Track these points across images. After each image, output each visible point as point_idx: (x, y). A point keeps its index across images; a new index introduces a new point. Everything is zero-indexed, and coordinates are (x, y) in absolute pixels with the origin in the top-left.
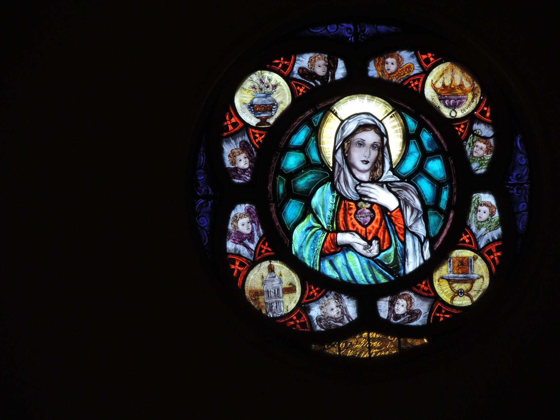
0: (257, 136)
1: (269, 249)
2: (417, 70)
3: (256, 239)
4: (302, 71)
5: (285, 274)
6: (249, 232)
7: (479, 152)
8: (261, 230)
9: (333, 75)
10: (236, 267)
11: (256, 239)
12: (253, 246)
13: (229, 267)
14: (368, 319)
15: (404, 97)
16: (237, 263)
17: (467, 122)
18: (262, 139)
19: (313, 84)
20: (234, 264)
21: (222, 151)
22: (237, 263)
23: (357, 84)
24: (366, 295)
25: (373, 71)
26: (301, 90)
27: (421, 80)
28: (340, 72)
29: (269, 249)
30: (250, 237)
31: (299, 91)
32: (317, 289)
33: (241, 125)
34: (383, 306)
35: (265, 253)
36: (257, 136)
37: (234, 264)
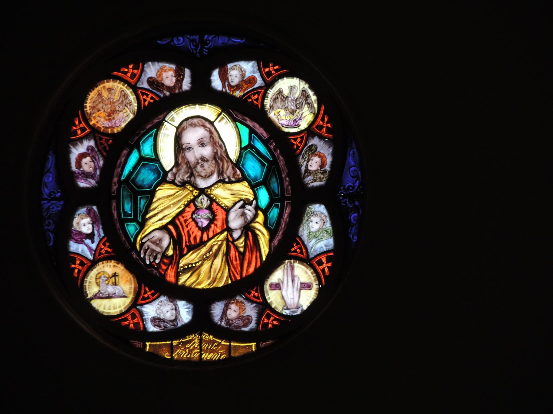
0: (298, 250)
1: (293, 141)
2: (260, 82)
3: (97, 239)
4: (151, 81)
5: (280, 116)
6: (90, 232)
7: (316, 163)
8: (101, 230)
9: (181, 87)
10: (77, 266)
11: (97, 239)
12: (94, 246)
13: (69, 266)
14: (202, 322)
15: (245, 108)
16: (78, 262)
17: (303, 136)
18: (293, 247)
19: (162, 96)
20: (75, 264)
21: (69, 152)
22: (78, 262)
23: (202, 93)
24: (201, 300)
25: (216, 82)
26: (148, 99)
27: (260, 100)
28: (186, 85)
29: (293, 141)
30: (91, 236)
31: (145, 100)
32: (250, 100)
33: (88, 130)
34: (217, 309)
35: (297, 138)
36: (298, 250)
37: (75, 264)
